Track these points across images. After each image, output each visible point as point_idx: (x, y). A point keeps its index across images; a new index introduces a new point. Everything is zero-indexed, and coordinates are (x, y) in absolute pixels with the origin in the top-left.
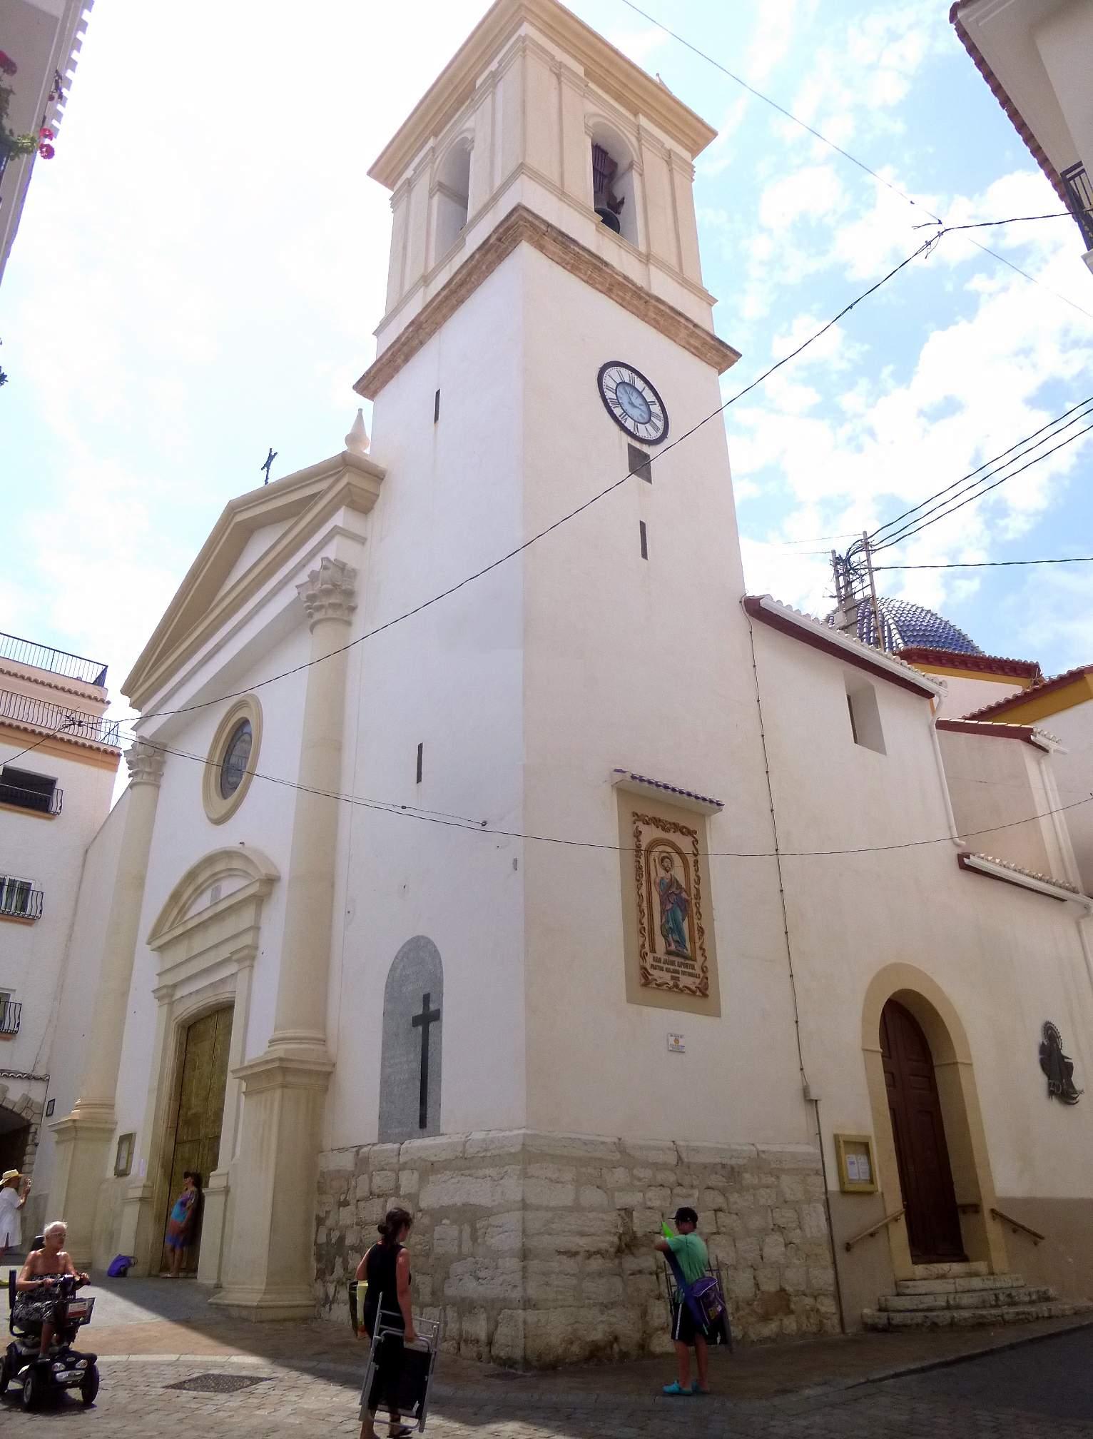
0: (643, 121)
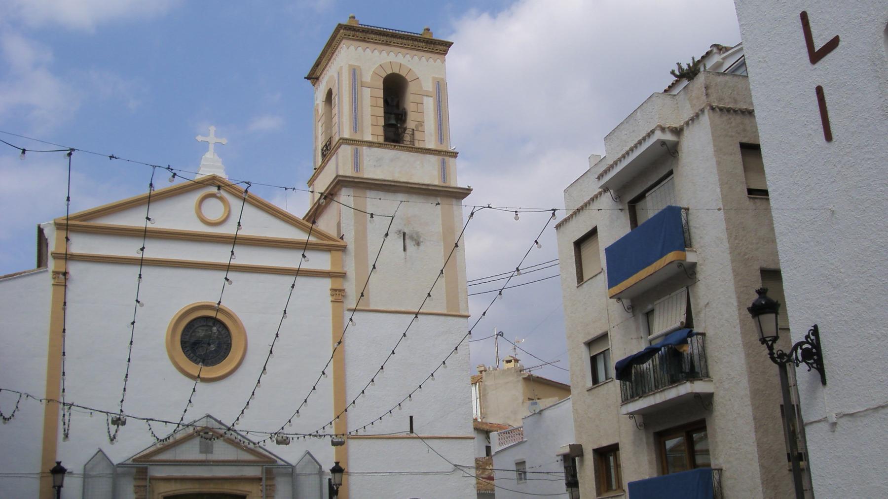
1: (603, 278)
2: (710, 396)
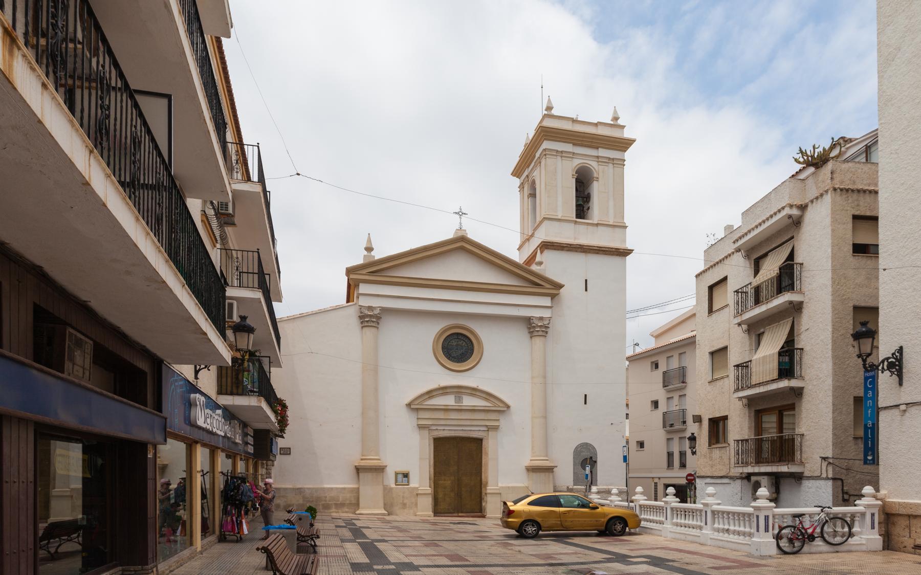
0: (602, 152)
1: (732, 309)
2: (802, 389)
